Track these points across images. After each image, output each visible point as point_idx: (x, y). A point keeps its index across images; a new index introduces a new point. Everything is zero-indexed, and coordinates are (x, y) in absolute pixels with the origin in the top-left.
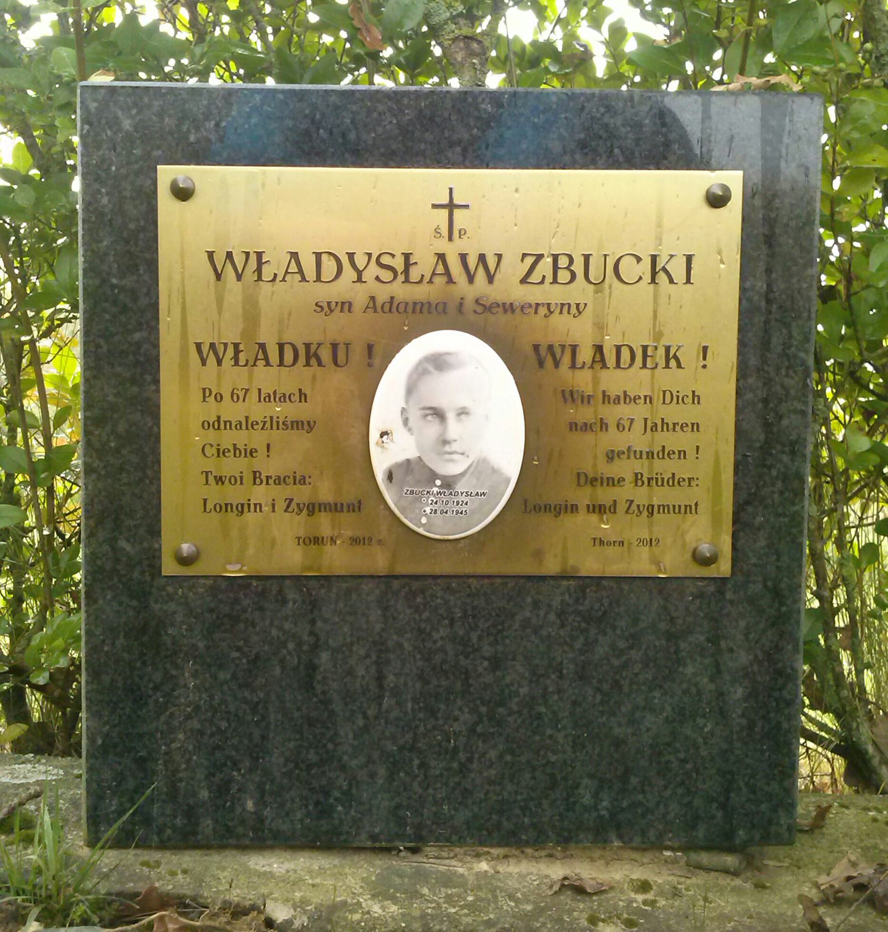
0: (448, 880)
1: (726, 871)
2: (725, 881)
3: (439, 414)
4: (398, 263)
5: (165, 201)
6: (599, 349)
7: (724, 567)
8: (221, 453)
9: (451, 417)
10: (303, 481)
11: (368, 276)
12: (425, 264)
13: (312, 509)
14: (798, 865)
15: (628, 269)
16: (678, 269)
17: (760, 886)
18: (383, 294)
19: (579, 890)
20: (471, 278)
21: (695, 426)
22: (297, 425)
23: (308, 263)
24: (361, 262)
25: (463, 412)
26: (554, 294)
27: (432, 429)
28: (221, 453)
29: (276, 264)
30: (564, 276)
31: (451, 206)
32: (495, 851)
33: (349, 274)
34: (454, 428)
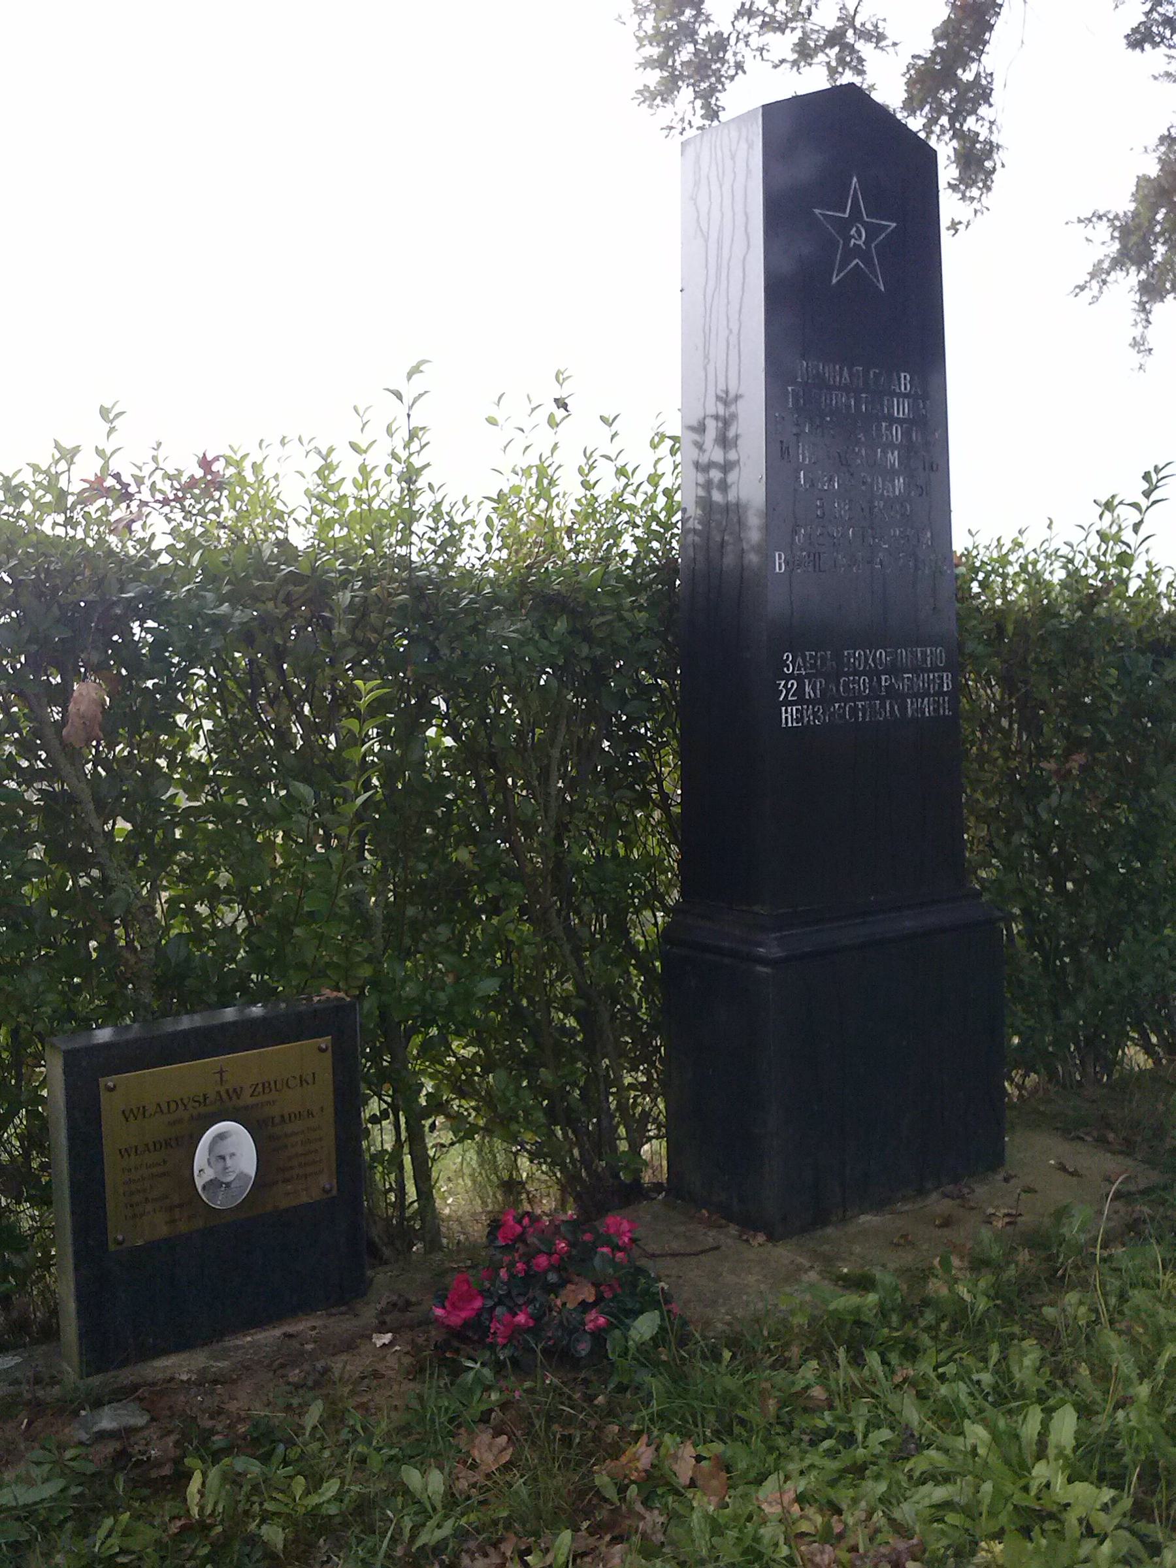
0: (238, 1348)
1: (342, 1314)
2: (342, 1317)
3: (223, 1158)
4: (201, 1099)
5: (104, 1095)
6: (282, 1116)
7: (334, 1192)
8: (132, 1194)
9: (228, 1158)
10: (167, 1197)
11: (189, 1107)
12: (212, 1096)
13: (171, 1209)
14: (368, 1304)
15: (292, 1083)
16: (310, 1080)
17: (356, 1315)
18: (195, 1113)
19: (290, 1336)
20: (230, 1098)
21: (321, 1139)
22: (164, 1174)
23: (164, 1107)
24: (185, 1101)
25: (233, 1155)
26: (266, 1098)
27: (221, 1164)
28: (132, 1194)
29: (151, 1109)
30: (267, 1090)
31: (221, 1072)
32: (252, 1331)
33: (181, 1107)
34: (229, 1162)
